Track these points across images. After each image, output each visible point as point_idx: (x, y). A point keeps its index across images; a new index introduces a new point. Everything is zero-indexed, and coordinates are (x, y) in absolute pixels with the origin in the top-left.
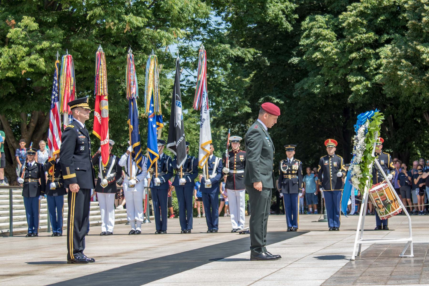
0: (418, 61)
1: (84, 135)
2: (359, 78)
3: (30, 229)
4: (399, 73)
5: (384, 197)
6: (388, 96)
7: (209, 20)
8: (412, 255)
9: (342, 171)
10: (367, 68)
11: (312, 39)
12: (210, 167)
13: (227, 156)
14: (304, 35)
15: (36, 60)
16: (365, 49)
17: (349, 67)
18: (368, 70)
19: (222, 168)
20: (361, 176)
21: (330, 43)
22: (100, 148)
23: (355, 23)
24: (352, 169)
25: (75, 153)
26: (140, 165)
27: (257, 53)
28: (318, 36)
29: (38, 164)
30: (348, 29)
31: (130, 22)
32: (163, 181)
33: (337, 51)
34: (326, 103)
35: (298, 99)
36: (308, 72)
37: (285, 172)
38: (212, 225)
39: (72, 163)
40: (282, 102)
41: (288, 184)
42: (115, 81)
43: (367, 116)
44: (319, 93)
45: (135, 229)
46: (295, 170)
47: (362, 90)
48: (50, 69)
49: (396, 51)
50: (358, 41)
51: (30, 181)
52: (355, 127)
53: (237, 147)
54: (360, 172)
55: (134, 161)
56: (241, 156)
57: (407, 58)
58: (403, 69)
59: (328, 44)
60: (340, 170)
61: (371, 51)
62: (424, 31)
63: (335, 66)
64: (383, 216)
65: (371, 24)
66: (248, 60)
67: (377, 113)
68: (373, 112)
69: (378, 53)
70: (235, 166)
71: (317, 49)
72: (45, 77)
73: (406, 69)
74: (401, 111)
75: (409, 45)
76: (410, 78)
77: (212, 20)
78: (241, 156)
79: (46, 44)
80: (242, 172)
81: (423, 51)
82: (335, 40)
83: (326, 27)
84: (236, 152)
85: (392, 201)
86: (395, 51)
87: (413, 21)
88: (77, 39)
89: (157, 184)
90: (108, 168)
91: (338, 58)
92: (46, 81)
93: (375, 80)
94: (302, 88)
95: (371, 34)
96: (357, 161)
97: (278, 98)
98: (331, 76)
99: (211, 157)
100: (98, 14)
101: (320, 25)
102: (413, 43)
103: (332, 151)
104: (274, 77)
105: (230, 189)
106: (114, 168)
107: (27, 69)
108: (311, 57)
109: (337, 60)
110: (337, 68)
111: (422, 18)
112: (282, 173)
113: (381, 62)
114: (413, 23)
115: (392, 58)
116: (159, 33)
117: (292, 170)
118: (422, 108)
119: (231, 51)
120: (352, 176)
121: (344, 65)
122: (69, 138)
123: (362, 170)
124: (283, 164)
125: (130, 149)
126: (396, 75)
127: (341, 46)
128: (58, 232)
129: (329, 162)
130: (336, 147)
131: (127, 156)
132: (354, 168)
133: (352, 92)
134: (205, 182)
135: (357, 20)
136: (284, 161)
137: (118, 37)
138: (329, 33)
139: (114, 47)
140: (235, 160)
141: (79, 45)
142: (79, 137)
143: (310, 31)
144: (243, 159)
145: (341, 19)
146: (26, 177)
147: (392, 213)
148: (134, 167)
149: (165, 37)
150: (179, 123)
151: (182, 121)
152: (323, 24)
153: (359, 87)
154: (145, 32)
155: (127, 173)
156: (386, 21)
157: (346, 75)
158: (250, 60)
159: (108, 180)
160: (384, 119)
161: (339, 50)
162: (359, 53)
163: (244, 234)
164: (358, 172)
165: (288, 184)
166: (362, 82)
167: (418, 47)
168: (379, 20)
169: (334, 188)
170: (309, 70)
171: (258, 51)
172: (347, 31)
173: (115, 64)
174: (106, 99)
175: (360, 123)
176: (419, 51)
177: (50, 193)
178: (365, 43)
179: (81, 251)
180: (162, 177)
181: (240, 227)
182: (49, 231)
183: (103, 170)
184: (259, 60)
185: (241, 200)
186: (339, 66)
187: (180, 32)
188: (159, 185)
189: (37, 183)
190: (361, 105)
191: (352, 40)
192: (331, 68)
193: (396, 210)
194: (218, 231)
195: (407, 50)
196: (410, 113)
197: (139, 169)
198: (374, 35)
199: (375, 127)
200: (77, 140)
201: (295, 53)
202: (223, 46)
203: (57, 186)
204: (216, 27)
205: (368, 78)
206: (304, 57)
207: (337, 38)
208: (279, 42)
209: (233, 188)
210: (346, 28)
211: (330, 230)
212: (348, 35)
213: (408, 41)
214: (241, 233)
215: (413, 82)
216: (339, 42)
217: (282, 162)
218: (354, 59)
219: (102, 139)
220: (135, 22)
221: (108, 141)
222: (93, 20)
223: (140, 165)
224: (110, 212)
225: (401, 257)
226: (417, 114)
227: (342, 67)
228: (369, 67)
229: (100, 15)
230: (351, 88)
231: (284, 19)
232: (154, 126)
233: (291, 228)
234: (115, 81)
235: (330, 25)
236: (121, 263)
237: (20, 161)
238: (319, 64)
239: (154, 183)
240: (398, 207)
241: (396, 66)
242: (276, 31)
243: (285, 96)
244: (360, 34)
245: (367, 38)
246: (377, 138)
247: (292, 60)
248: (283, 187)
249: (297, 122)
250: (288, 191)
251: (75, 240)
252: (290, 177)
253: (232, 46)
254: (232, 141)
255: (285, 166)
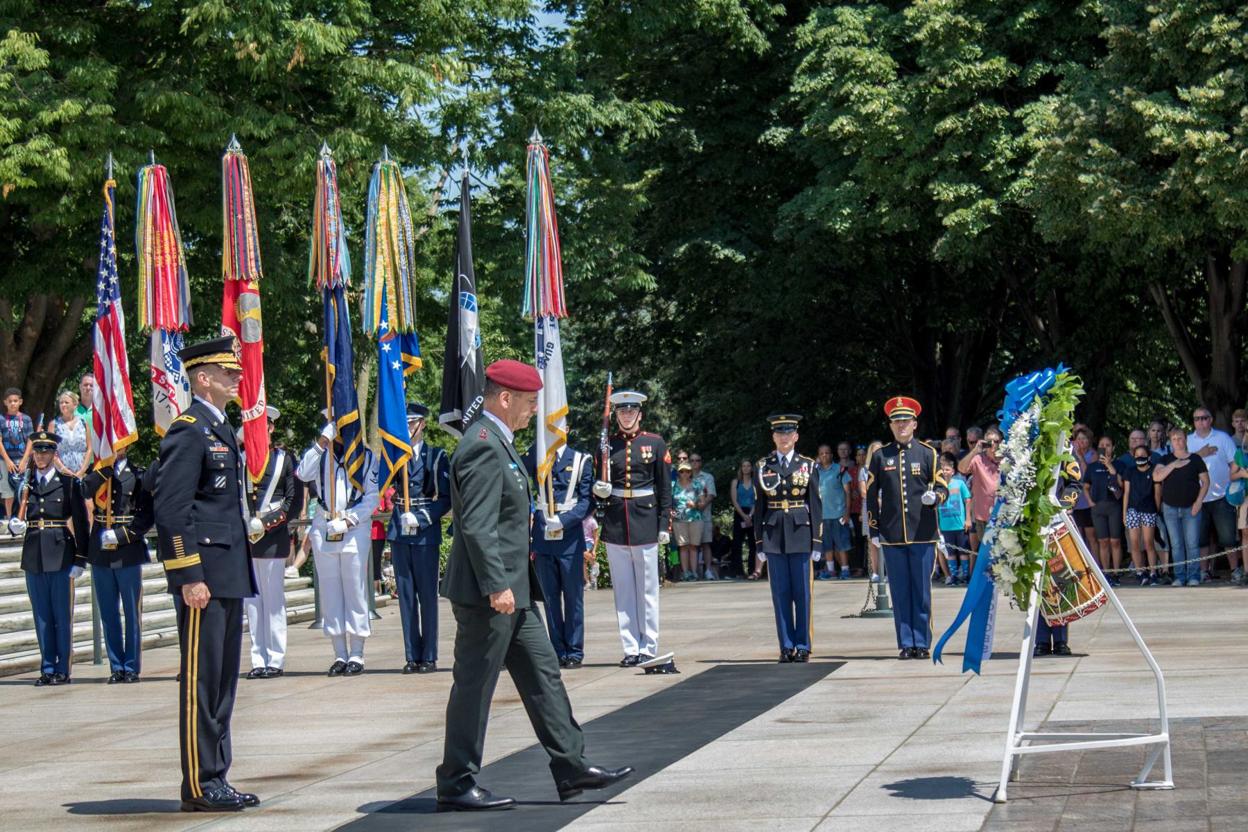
0: (1135, 142)
1: (225, 443)
2: (963, 190)
3: (46, 663)
4: (1083, 178)
5: (1058, 563)
6: (1046, 240)
7: (529, 25)
8: (1169, 783)
9: (934, 490)
10: (986, 162)
11: (828, 77)
12: (558, 480)
13: (605, 447)
14: (804, 64)
15: (43, 152)
16: (982, 105)
17: (936, 159)
18: (989, 167)
19: (592, 483)
20: (1021, 559)
21: (880, 88)
22: (241, 430)
23: (952, 29)
24: (995, 539)
25: (198, 497)
26: (359, 477)
27: (668, 114)
28: (843, 67)
29: (64, 478)
30: (929, 46)
31: (307, 41)
32: (425, 520)
33: (900, 113)
34: (868, 257)
35: (788, 247)
36: (814, 170)
37: (772, 491)
38: (566, 645)
39: (188, 524)
40: (740, 258)
41: (779, 525)
42: (285, 249)
43: (1035, 385)
44: (849, 231)
45: (348, 658)
46: (800, 487)
47: (974, 223)
48: (82, 177)
49: (1073, 113)
50: (960, 83)
51: (42, 524)
52: (1001, 417)
53: (631, 423)
54: (1018, 549)
55: (341, 465)
56: (643, 448)
57: (1104, 133)
58: (1094, 167)
59: (874, 91)
60: (931, 485)
61: (996, 110)
62: (1154, 56)
63: (893, 154)
64: (1055, 616)
65: (998, 32)
66: (644, 136)
67: (1063, 375)
68: (1050, 373)
69: (1021, 119)
70: (629, 476)
71: (841, 104)
72: (64, 200)
73: (1104, 166)
74: (1083, 278)
75: (1109, 97)
76: (1115, 192)
77: (538, 25)
78: (643, 448)
79: (70, 107)
80: (649, 492)
81: (1151, 116)
82: (893, 78)
83: (867, 41)
84: (630, 437)
85: (1080, 574)
86: (1068, 113)
87: (1122, 29)
88: (156, 91)
89: (408, 530)
90: (263, 486)
91: (902, 132)
92: (68, 209)
93: (1012, 194)
94: (800, 218)
95: (999, 63)
96: (1010, 518)
97: (727, 244)
98: (883, 183)
99: (561, 451)
100: (214, 15)
101: (849, 37)
102: (1122, 90)
103: (906, 432)
104: (716, 183)
105: (614, 542)
106: (282, 485)
107: (19, 181)
108: (826, 128)
109: (900, 137)
110: (900, 162)
111: (1150, 19)
112: (764, 496)
113: (1026, 142)
114: (1121, 33)
115: (1062, 134)
116: (391, 68)
117: (791, 486)
118: (1146, 270)
119: (595, 114)
120: (996, 561)
121: (922, 152)
122: (181, 454)
123: (1024, 545)
124: (766, 470)
125: (329, 432)
126: (1072, 183)
127: (909, 95)
128: (128, 668)
129: (897, 463)
130: (919, 419)
131: (319, 452)
132: (1002, 537)
133: (945, 228)
134: (544, 524)
135: (957, 22)
136: (769, 461)
137: (273, 82)
138: (875, 59)
139: (263, 113)
140: (629, 459)
141: (161, 108)
142: (212, 449)
143: (819, 54)
144: (650, 455)
145: (912, 20)
146: (32, 514)
147: (1081, 606)
148: (340, 484)
149: (408, 80)
150: (470, 356)
151: (477, 351)
152: (857, 34)
153: (965, 214)
154: (353, 67)
155: (321, 502)
156: (1042, 22)
157: (925, 181)
158: (650, 135)
159: (264, 521)
160: (1082, 392)
161: (904, 110)
162: (964, 117)
163: (659, 672)
164: (1012, 550)
165: (779, 525)
166: (975, 201)
167: (1139, 105)
168: (1022, 20)
169: (913, 534)
170: (817, 163)
171: (673, 109)
172: (929, 55)
173: (266, 159)
174: (253, 291)
175: (1014, 407)
176: (1140, 114)
177: (101, 560)
178: (979, 89)
179: (221, 774)
180: (424, 511)
181: (645, 651)
182: (97, 661)
183: (250, 491)
184: (674, 135)
185: (647, 573)
186: (906, 155)
187: (452, 67)
188: (414, 533)
189: (61, 531)
190: (971, 264)
191: (942, 80)
192: (884, 159)
193: (1093, 599)
194: (583, 662)
195: (1104, 111)
196: (1108, 283)
197: (355, 489)
198: (1006, 65)
199: (1060, 418)
200: (205, 458)
201: (774, 112)
202: (573, 98)
203: (121, 538)
204: (551, 44)
205: (990, 191)
206: (805, 129)
207: (900, 73)
208: (729, 82)
209: (625, 539)
210: (925, 44)
211: (902, 657)
212: (932, 66)
213: (1106, 81)
214: (649, 670)
215: (1123, 205)
216: (905, 83)
217: (762, 464)
218: (950, 133)
219: (246, 404)
220: (320, 40)
221: (262, 409)
222: (200, 31)
223: (359, 477)
224: (274, 613)
225: (1138, 789)
226: (1131, 286)
227: (915, 156)
228: (992, 157)
229: (219, 19)
230: (941, 219)
231: (746, 19)
232: (396, 365)
233: (792, 651)
234: (285, 249)
235: (878, 36)
236: (338, 811)
237: (8, 451)
238: (849, 149)
239: (399, 528)
240: (1099, 589)
241: (1073, 158)
242: (720, 50)
243: (749, 237)
244: (967, 62)
245: (986, 74)
246: (1065, 449)
247: (767, 134)
248: (765, 534)
249: (783, 313)
250: (782, 547)
251: (203, 747)
252: (785, 505)
253: (600, 97)
254: (618, 406)
255: (770, 474)
